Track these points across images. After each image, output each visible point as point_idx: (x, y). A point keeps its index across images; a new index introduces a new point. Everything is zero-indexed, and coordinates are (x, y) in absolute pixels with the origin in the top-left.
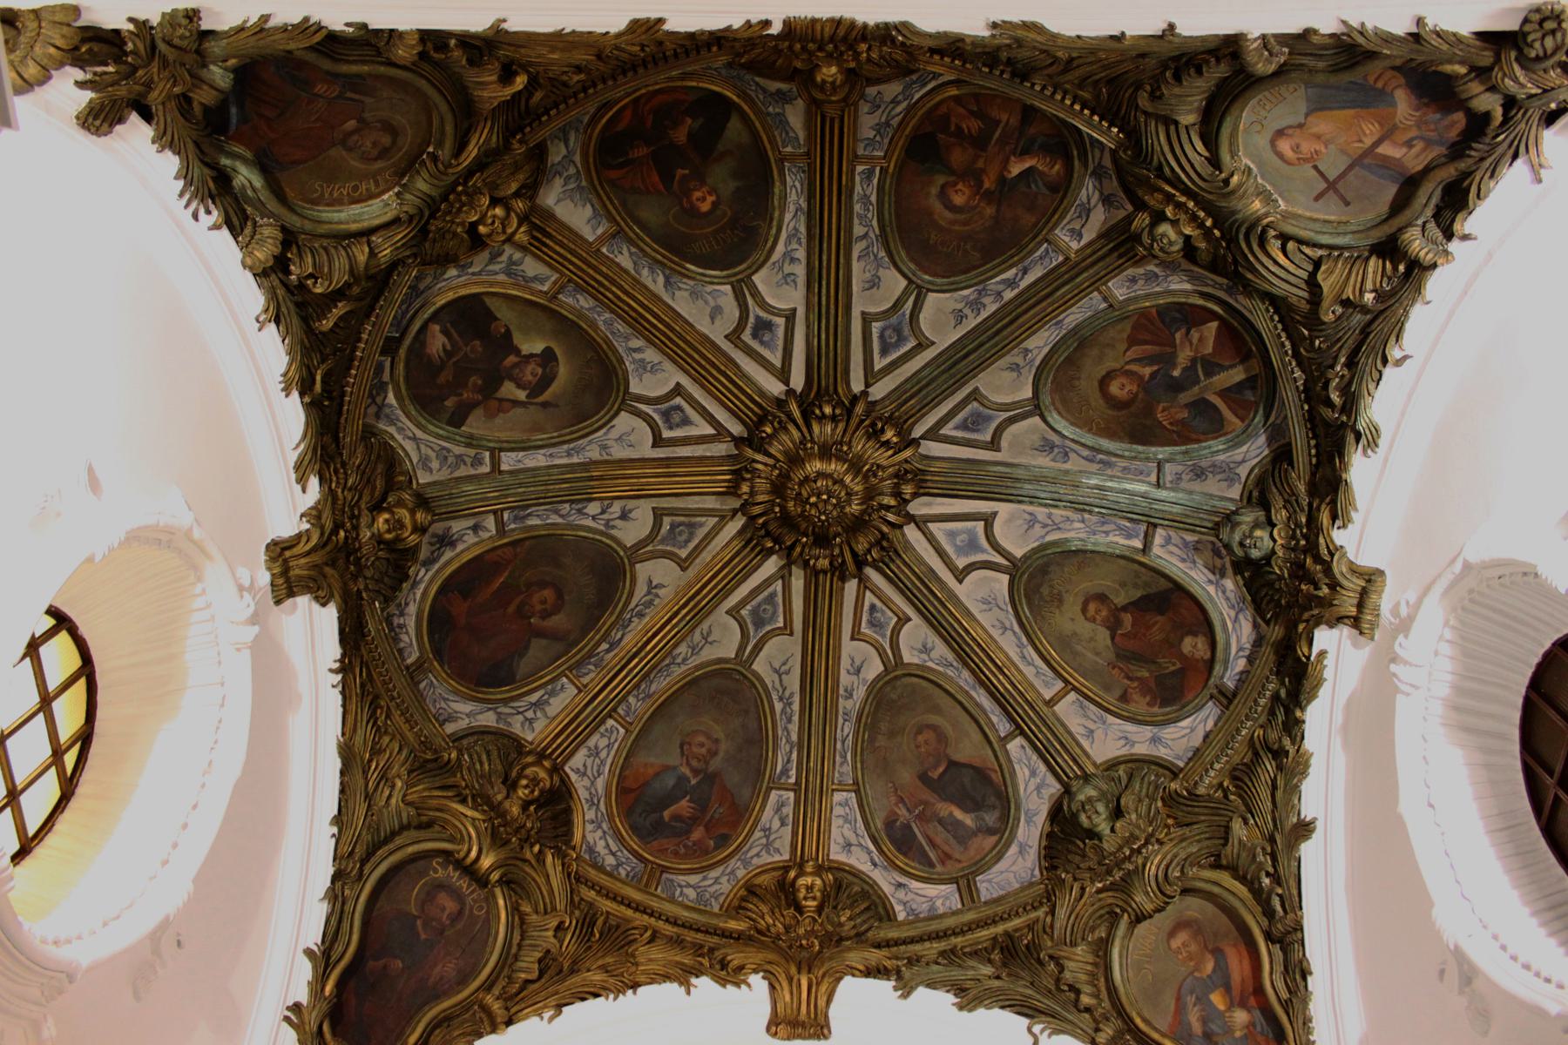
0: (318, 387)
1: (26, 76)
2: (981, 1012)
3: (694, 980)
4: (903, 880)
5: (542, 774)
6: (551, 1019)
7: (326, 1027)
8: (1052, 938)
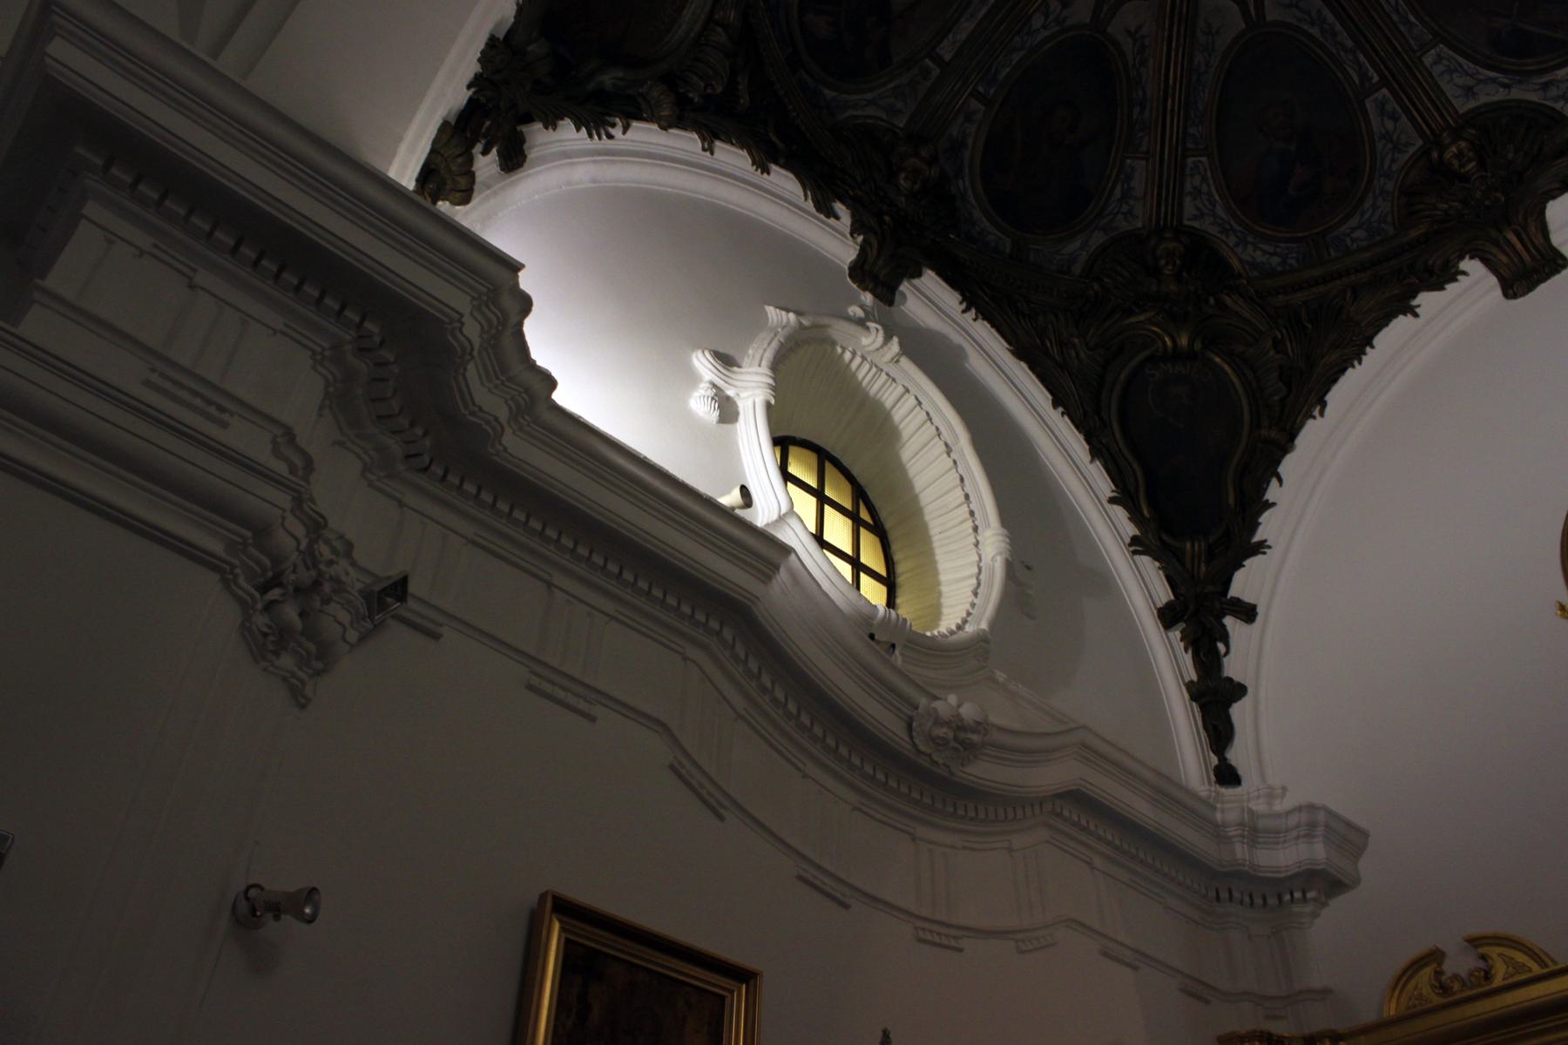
0: (780, 145)
1: (464, 188)
3: (1414, 303)
5: (1172, 245)
6: (1322, 414)
7: (1165, 537)
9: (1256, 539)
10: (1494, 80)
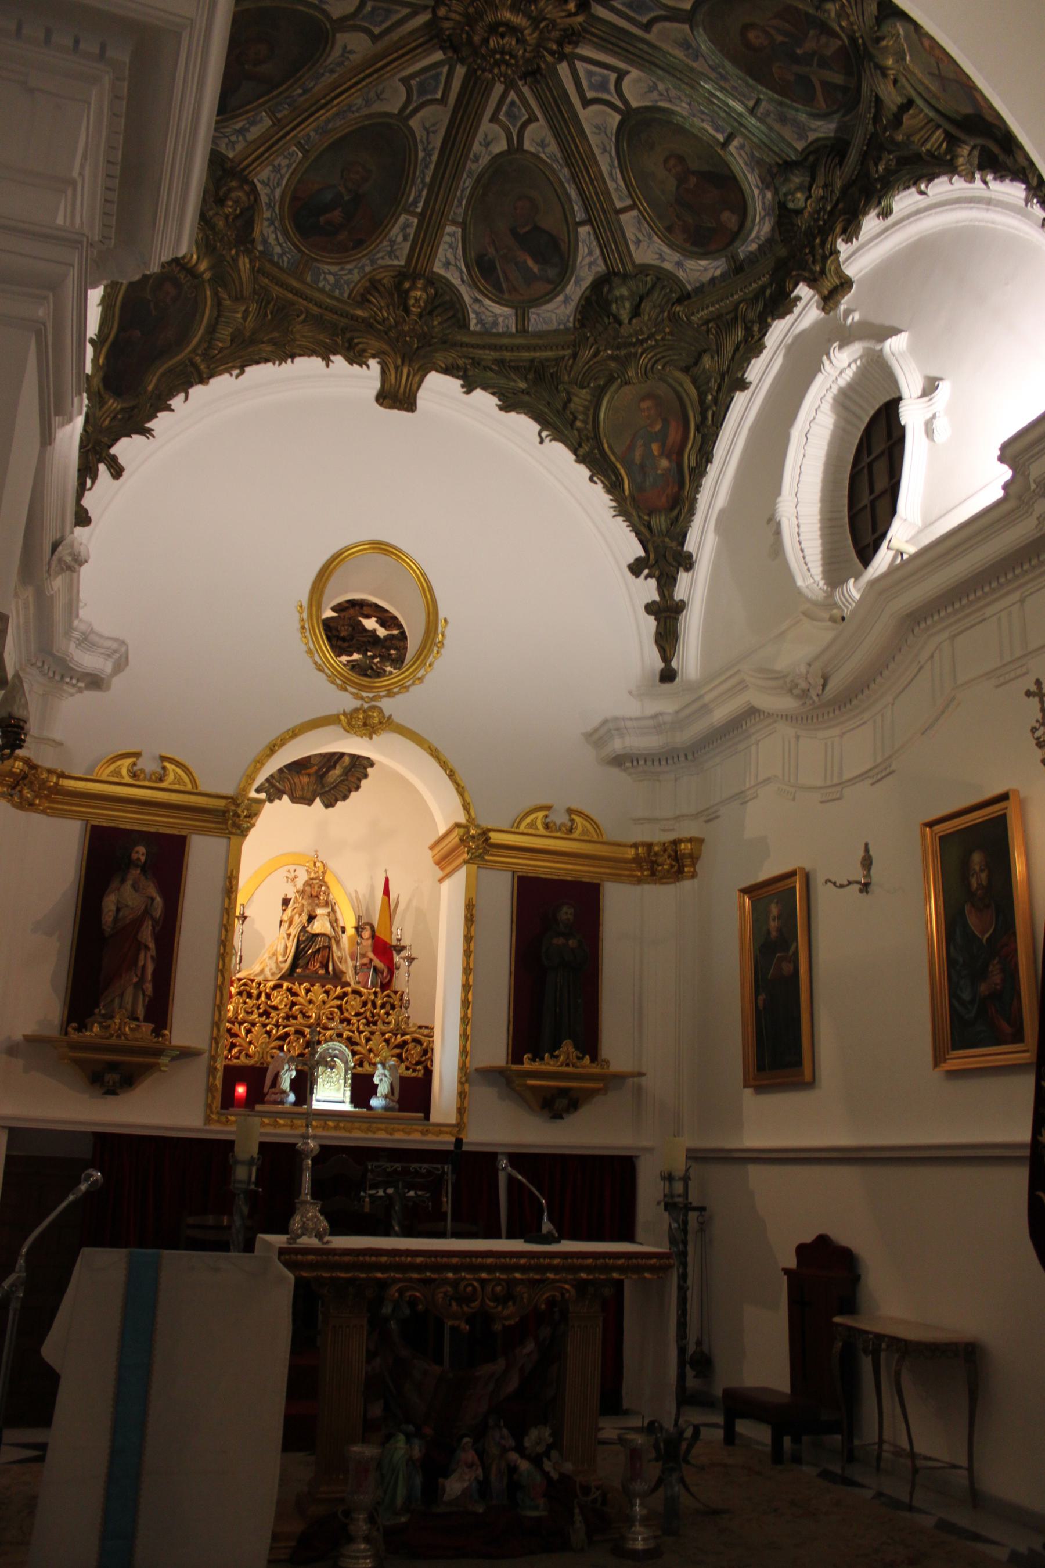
2: (513, 415)
3: (332, 358)
4: (480, 297)
5: (244, 198)
6: (237, 377)
8: (569, 374)
9: (149, 425)
10: (461, 272)
